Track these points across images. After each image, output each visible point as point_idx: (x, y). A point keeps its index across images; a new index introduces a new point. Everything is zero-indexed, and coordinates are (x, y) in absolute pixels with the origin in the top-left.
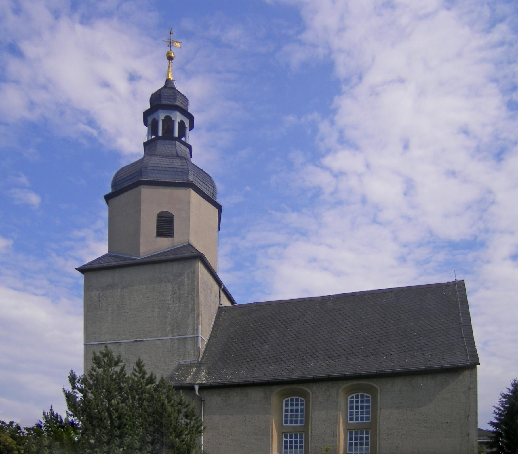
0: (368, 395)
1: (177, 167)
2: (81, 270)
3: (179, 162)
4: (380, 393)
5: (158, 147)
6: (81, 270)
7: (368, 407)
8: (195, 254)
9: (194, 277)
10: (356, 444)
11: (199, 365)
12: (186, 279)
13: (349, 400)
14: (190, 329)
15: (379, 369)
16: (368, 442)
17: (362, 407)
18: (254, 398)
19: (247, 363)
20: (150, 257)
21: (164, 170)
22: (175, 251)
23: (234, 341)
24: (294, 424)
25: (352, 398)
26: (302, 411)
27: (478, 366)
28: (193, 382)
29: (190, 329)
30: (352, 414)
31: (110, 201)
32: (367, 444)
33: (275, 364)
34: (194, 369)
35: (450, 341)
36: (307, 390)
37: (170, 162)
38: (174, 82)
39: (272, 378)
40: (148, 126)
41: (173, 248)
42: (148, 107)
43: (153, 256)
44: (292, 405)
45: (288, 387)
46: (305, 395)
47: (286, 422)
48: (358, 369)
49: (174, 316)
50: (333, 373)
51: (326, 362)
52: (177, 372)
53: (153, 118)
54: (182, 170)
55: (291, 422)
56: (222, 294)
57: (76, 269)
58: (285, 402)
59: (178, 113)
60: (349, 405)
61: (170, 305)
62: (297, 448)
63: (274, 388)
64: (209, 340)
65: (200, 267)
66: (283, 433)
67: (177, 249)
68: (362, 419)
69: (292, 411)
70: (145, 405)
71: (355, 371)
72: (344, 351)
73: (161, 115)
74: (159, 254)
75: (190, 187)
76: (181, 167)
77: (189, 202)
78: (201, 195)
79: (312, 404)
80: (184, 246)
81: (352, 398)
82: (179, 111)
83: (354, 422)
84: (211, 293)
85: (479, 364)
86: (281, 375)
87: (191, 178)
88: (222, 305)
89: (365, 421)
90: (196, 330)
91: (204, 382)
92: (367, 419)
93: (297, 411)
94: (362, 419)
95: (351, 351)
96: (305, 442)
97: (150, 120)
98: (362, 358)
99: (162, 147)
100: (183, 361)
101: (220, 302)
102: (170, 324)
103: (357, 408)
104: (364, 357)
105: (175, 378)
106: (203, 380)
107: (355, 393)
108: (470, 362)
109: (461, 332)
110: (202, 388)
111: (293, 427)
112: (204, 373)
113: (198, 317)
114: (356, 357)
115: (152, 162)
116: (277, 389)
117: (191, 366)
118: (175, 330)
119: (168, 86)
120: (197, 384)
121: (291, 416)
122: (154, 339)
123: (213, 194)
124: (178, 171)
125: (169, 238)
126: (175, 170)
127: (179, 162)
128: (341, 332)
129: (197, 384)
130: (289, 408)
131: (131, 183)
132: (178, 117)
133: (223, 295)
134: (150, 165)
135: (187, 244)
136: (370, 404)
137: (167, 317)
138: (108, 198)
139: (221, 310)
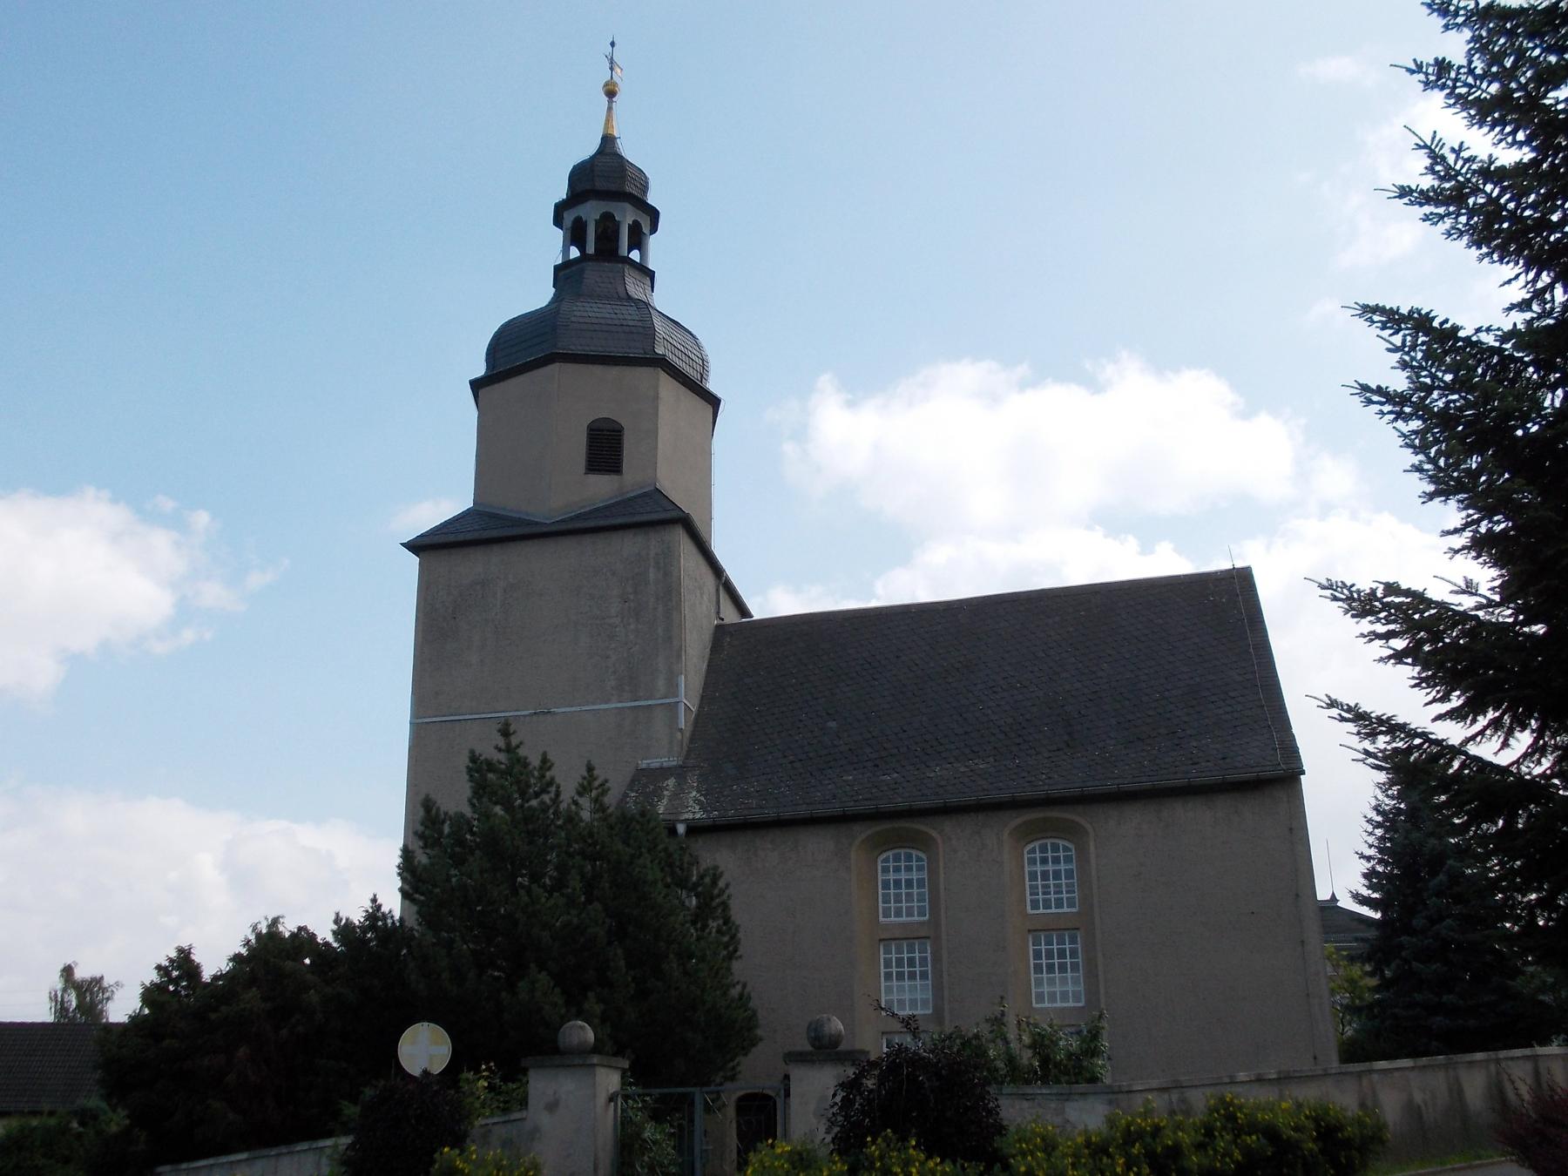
0: (1067, 844)
1: (631, 323)
2: (415, 546)
3: (634, 312)
4: (1095, 841)
5: (585, 276)
6: (415, 546)
7: (1069, 874)
8: (673, 514)
9: (666, 564)
10: (1051, 968)
11: (680, 772)
12: (651, 570)
13: (1026, 856)
14: (661, 683)
15: (1089, 784)
16: (1078, 963)
17: (1057, 875)
18: (813, 854)
19: (790, 765)
20: (572, 519)
21: (602, 331)
22: (625, 504)
23: (758, 711)
24: (904, 919)
25: (1033, 851)
26: (921, 883)
27: (1302, 777)
28: (671, 817)
29: (661, 683)
30: (1036, 891)
31: (481, 392)
32: (1075, 967)
33: (855, 769)
34: (671, 782)
35: (1236, 715)
36: (923, 828)
37: (616, 314)
38: (618, 140)
39: (852, 804)
40: (564, 227)
41: (619, 499)
42: (561, 193)
43: (578, 517)
44: (897, 870)
45: (887, 826)
46: (923, 843)
47: (887, 915)
48: (1041, 783)
49: (625, 655)
50: (986, 793)
51: (967, 764)
52: (632, 791)
53: (576, 215)
54: (641, 330)
55: (898, 913)
56: (722, 594)
57: (401, 544)
58: (1028, 853)
59: (628, 206)
60: (1027, 869)
61: (616, 627)
62: (915, 979)
63: (856, 828)
64: (701, 706)
65: (686, 547)
66: (881, 940)
67: (629, 499)
68: (1059, 904)
69: (897, 883)
70: (472, 818)
71: (1034, 789)
72: (1006, 735)
73: (591, 212)
74: (590, 512)
75: (658, 367)
76: (640, 324)
77: (656, 398)
78: (681, 380)
79: (945, 868)
80: (645, 495)
81: (1033, 851)
82: (630, 203)
83: (1041, 911)
84: (702, 594)
85: (1304, 774)
86: (870, 796)
87: (659, 350)
88: (723, 619)
89: (1065, 910)
90: (672, 688)
91: (698, 816)
92: (1071, 904)
93: (909, 883)
94: (1059, 904)
95: (1020, 736)
96: (878, 912)
97: (569, 218)
98: (1046, 755)
99: (594, 275)
100: (644, 764)
101: (718, 613)
102: (614, 672)
103: (1045, 875)
104: (1050, 751)
105: (630, 807)
106: (694, 812)
107: (1037, 839)
108: (1283, 767)
109: (1258, 693)
110: (694, 830)
111: (903, 925)
112: (694, 793)
113: (679, 656)
114: (1033, 752)
115: (578, 314)
116: (863, 832)
117: (664, 772)
118: (627, 688)
119: (607, 151)
120: (682, 821)
121: (898, 899)
122: (578, 709)
123: (702, 376)
124: (632, 333)
125: (614, 477)
126: (627, 329)
127: (634, 312)
128: (994, 689)
129: (682, 821)
130: (892, 877)
131: (532, 358)
132: (626, 216)
133: (723, 594)
134: (573, 319)
135: (653, 488)
136: (1073, 866)
137: (608, 657)
138: (476, 385)
139: (721, 631)
